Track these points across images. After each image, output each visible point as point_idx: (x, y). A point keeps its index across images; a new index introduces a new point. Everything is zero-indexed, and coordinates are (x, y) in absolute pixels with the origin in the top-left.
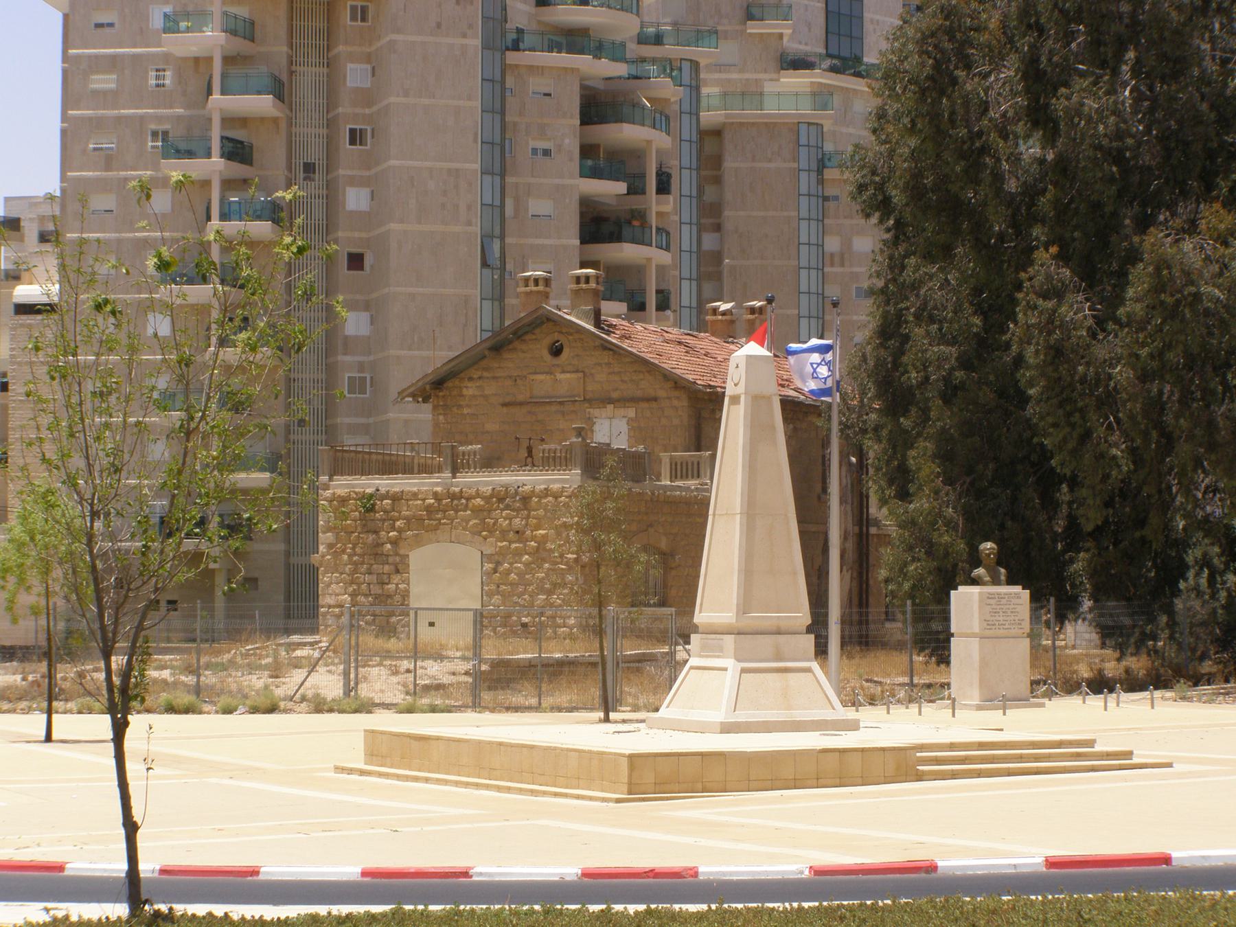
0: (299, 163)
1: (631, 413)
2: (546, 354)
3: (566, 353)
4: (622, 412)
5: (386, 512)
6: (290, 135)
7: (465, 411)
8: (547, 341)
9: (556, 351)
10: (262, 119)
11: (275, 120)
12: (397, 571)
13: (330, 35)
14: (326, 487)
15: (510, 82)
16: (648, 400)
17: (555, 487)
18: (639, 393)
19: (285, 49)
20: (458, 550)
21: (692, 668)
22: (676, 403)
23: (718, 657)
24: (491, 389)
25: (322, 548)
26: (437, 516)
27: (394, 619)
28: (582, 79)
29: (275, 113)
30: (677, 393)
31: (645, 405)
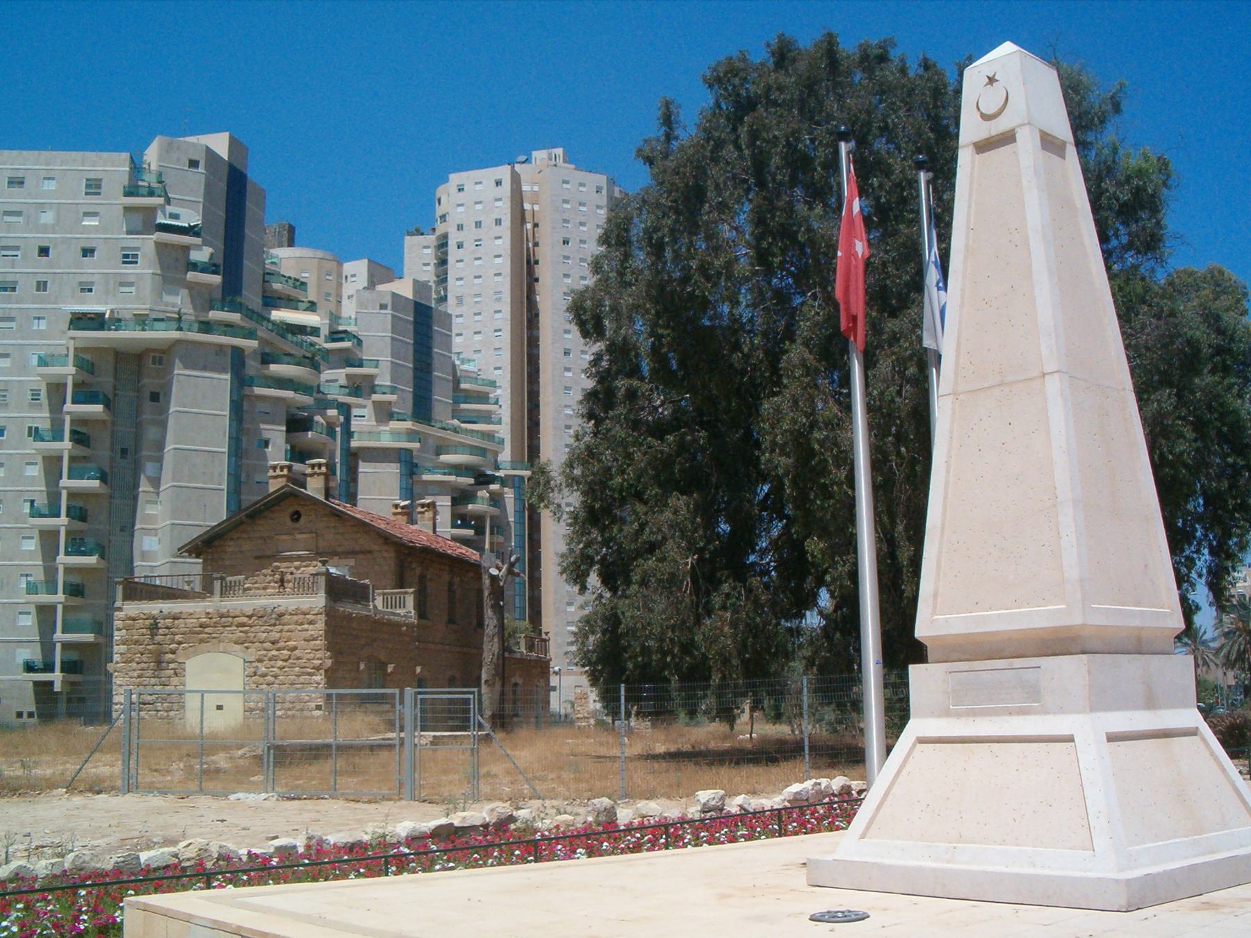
0: (118, 448)
1: (352, 562)
2: (288, 520)
3: (302, 520)
4: (345, 561)
5: (167, 628)
6: (113, 432)
7: (227, 563)
8: (291, 510)
9: (296, 517)
10: (96, 421)
11: (104, 422)
12: (176, 674)
13: (138, 412)
14: (120, 609)
15: (246, 405)
16: (362, 552)
17: (305, 607)
18: (357, 548)
19: (111, 379)
20: (226, 658)
21: (922, 741)
22: (386, 554)
23: (1022, 712)
24: (247, 546)
25: (116, 657)
26: (204, 634)
27: (172, 713)
28: (288, 407)
29: (105, 417)
30: (386, 547)
31: (361, 556)
